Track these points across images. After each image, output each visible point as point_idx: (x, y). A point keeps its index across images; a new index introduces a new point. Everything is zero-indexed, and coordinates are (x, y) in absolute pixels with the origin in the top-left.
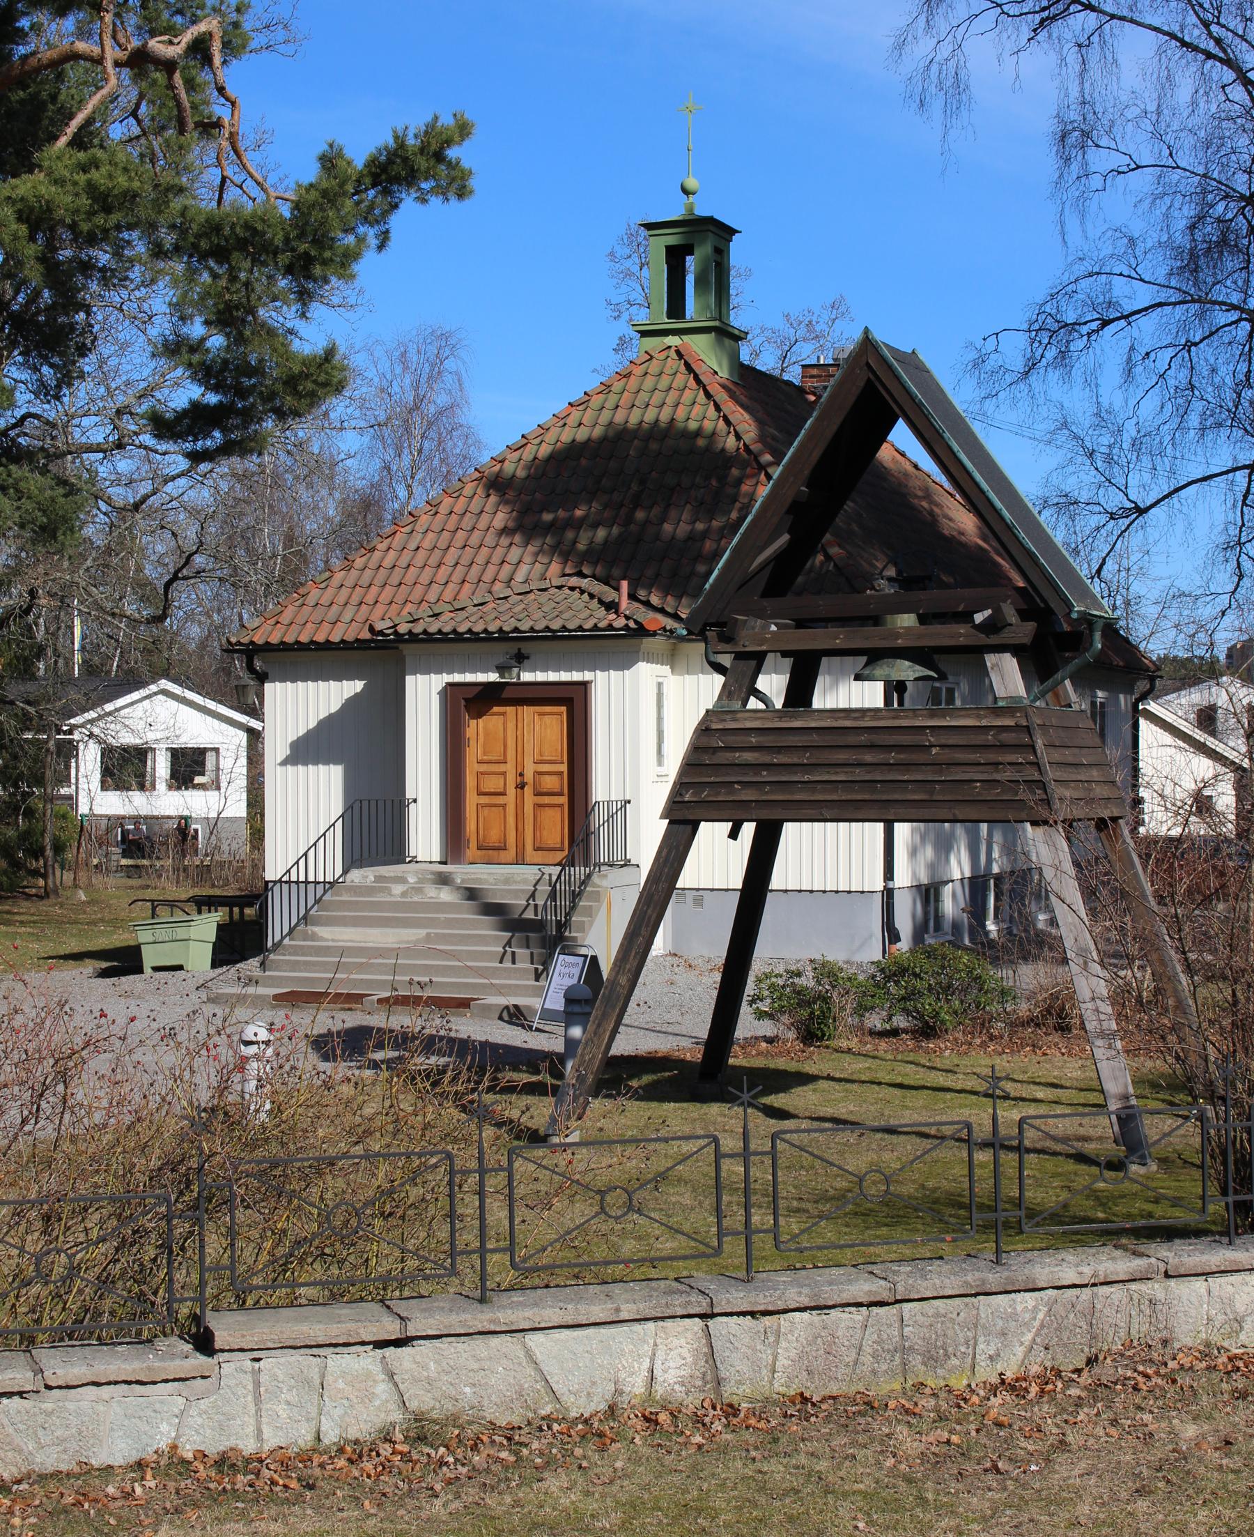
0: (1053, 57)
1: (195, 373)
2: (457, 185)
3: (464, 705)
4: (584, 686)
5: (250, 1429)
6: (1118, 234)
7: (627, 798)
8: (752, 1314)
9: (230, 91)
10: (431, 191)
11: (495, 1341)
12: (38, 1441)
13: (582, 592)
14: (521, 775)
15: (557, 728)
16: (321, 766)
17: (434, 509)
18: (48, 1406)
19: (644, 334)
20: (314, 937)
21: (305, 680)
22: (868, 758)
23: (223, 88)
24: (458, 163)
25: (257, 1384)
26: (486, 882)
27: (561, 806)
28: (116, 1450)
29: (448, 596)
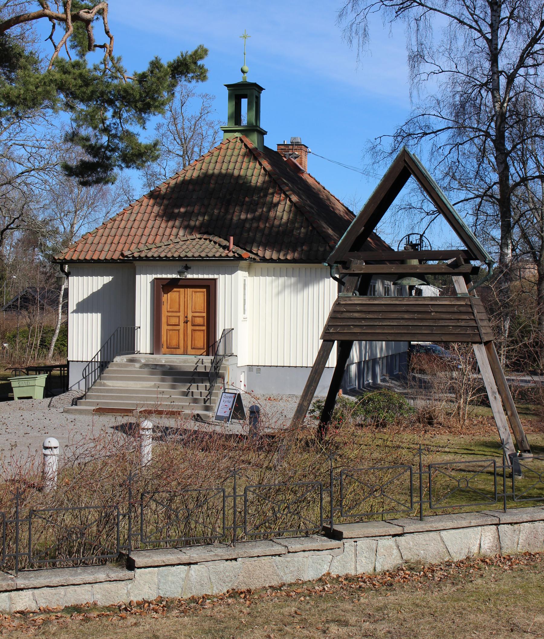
0: (406, 24)
1: (87, 149)
2: (202, 76)
3: (161, 288)
4: (215, 280)
5: (353, 567)
6: (432, 98)
7: (232, 328)
8: (511, 524)
9: (111, 34)
10: (192, 78)
11: (431, 534)
12: (285, 572)
13: (210, 241)
14: (186, 317)
15: (202, 298)
16: (89, 314)
17: (140, 204)
18: (288, 559)
19: (226, 131)
20: (104, 385)
21: (87, 275)
22: (406, 316)
23: (109, 32)
24: (203, 66)
25: (356, 550)
26: (176, 362)
27: (203, 330)
28: (310, 575)
29: (151, 240)
